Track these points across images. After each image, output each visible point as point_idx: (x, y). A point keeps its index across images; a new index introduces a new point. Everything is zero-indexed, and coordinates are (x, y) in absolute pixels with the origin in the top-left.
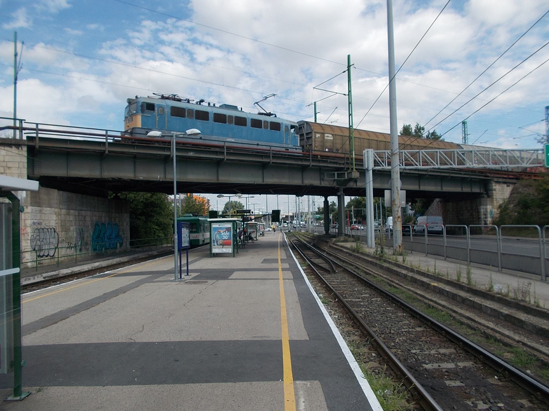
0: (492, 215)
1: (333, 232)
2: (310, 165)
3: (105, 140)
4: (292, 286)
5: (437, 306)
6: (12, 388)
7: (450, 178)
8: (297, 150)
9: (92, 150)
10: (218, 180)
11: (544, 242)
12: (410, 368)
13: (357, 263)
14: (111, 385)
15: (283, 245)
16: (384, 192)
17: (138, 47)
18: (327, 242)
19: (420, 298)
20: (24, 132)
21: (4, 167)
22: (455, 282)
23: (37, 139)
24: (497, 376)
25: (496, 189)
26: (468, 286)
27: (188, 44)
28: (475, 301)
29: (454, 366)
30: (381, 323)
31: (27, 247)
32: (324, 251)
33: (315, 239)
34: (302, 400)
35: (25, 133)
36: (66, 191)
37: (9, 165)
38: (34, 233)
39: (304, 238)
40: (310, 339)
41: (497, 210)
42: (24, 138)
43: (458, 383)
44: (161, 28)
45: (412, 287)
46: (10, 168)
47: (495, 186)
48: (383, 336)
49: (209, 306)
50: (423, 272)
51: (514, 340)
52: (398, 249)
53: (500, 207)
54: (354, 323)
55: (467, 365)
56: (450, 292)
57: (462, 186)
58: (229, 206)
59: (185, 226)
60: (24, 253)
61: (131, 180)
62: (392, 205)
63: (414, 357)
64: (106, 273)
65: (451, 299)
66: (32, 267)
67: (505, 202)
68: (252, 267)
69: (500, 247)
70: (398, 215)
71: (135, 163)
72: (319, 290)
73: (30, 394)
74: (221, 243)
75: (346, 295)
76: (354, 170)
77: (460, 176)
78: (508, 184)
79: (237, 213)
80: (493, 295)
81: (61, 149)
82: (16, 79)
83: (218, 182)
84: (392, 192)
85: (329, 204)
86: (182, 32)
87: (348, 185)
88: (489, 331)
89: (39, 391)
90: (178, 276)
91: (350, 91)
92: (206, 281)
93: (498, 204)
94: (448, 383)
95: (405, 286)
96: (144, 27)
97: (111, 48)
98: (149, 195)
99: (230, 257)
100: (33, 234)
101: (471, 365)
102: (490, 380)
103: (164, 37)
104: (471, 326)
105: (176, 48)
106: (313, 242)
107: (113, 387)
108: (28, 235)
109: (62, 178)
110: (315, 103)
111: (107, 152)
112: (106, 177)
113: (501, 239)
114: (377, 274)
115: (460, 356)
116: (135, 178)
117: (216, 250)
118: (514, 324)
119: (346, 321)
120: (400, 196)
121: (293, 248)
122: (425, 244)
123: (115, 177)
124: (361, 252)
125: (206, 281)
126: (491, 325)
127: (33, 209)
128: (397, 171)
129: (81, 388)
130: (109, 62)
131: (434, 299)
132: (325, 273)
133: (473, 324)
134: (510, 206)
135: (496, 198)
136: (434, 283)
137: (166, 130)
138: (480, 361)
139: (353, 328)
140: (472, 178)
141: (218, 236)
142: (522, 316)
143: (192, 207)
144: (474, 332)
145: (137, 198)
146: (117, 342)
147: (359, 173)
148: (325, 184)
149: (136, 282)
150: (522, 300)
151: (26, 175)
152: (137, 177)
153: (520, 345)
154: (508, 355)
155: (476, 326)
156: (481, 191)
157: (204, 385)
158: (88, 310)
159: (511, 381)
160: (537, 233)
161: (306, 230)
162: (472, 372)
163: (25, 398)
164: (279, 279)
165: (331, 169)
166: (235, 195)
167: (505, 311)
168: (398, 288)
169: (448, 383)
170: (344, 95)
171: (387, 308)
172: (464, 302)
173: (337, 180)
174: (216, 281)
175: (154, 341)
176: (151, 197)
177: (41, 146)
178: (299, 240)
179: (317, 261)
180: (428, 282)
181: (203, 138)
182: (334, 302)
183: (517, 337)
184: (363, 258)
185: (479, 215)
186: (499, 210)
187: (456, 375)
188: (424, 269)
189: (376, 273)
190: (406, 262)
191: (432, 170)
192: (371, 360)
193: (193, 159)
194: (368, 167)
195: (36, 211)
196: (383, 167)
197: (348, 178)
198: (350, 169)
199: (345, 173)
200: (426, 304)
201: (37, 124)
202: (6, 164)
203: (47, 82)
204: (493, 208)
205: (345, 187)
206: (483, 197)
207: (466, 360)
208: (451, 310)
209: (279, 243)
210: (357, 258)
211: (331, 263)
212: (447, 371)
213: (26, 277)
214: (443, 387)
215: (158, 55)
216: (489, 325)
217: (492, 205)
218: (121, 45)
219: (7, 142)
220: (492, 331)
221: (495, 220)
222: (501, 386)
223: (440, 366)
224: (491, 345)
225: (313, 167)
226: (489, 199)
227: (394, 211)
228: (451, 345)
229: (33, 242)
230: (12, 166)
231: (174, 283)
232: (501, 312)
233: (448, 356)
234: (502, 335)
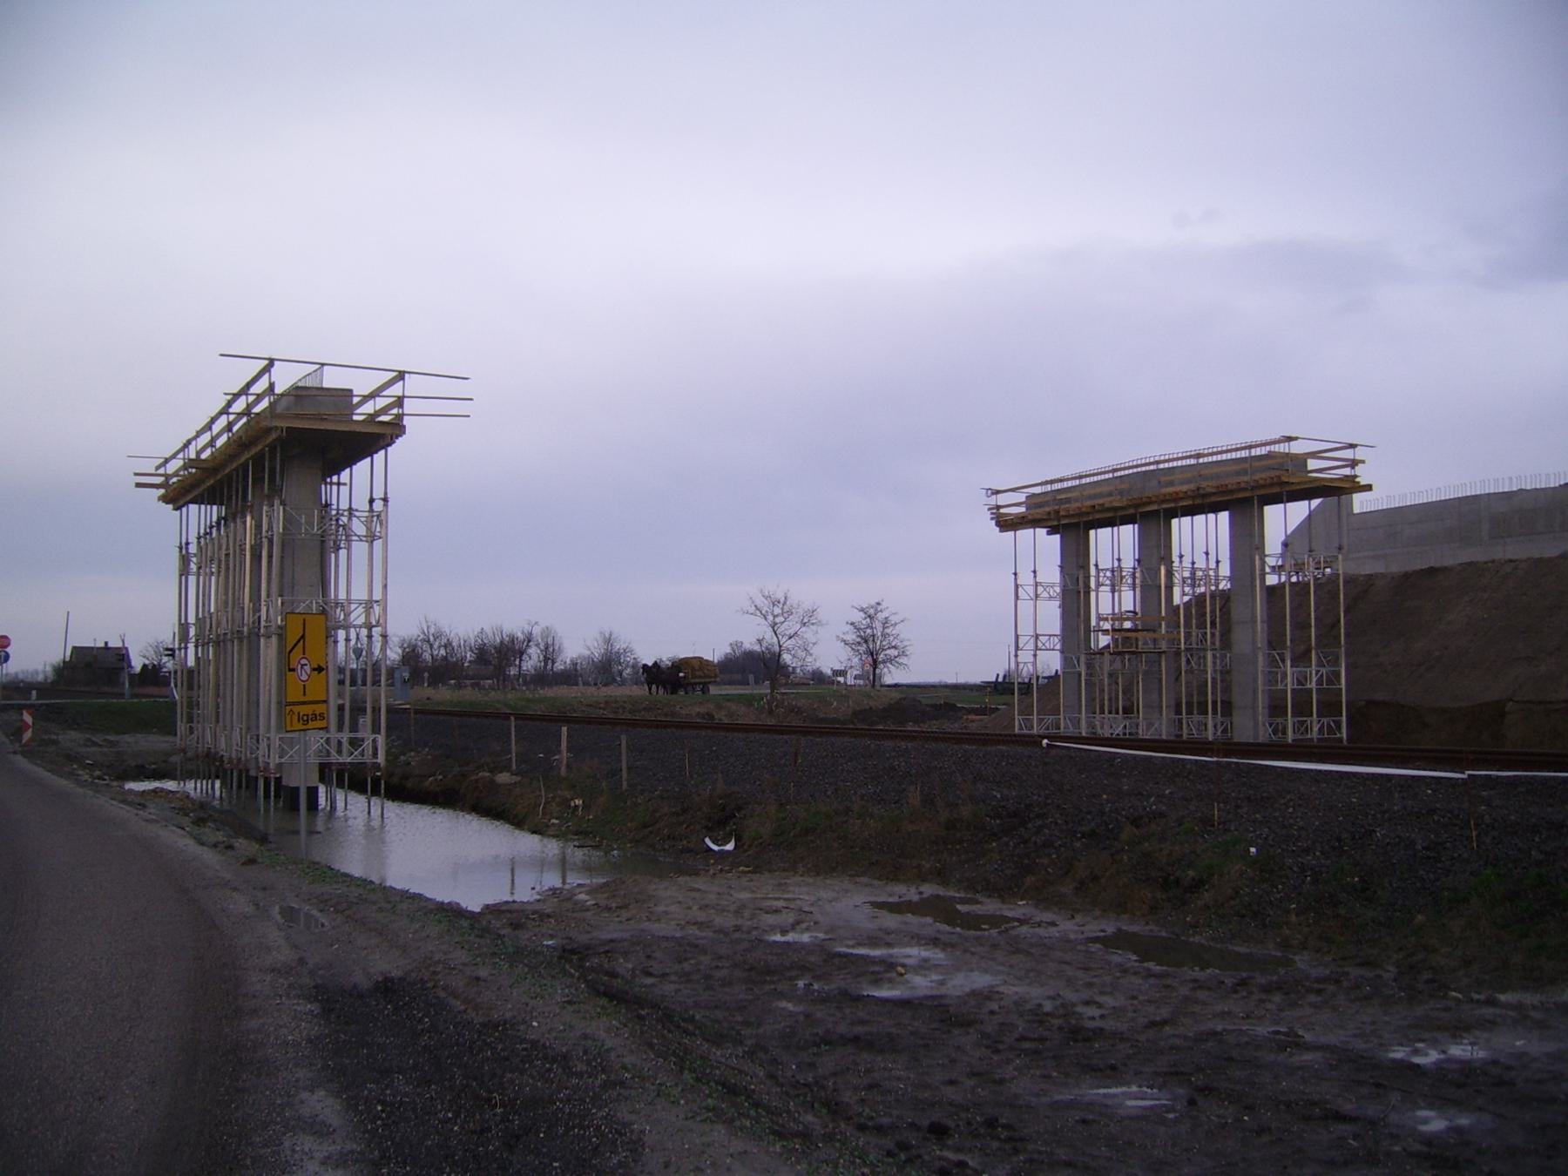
3: (345, 597)
8: (190, 541)
35: (292, 725)
118: (339, 721)
130: (1226, 673)
137: (1251, 465)
183: (211, 657)
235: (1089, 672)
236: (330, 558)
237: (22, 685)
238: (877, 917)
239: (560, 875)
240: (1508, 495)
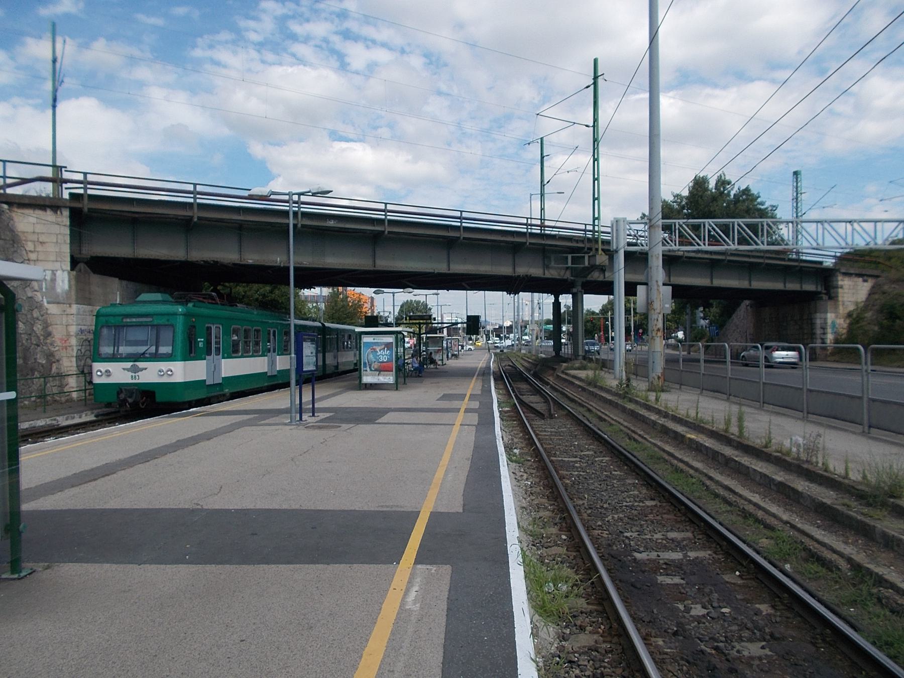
0: (835, 330)
1: (568, 354)
2: (526, 243)
4: (470, 436)
5: (687, 469)
7: (726, 262)
9: (172, 216)
10: (375, 266)
11: (869, 371)
12: (612, 557)
13: (591, 403)
14: (150, 564)
15: (484, 373)
16: (636, 288)
17: (255, 45)
18: (554, 369)
19: (667, 457)
20: (65, 186)
21: (34, 241)
22: (721, 433)
23: (86, 199)
24: (740, 572)
25: (844, 287)
26: (738, 440)
27: (336, 39)
28: (743, 462)
29: (681, 557)
30: (595, 494)
31: (72, 368)
32: (548, 384)
33: (537, 365)
34: (416, 588)
35: (66, 188)
36: (133, 281)
37: (42, 238)
38: (82, 346)
39: (522, 362)
40: (464, 512)
41: (844, 321)
42: (66, 195)
43: (677, 580)
44: (290, 13)
45: (660, 441)
46: (44, 243)
47: (842, 280)
48: (589, 511)
49: (330, 462)
50: (679, 418)
51: (780, 520)
52: (655, 383)
53: (849, 315)
54: (552, 493)
55: (700, 556)
56: (710, 448)
57: (785, 279)
58: (407, 308)
59: (309, 339)
60: (66, 377)
61: (235, 264)
62: (648, 309)
63: (623, 541)
64: (191, 410)
65: (710, 459)
66: (79, 399)
67: (858, 308)
68: (420, 406)
69: (807, 380)
70: (658, 327)
71: (240, 237)
72: (516, 443)
73: (34, 571)
74: (376, 367)
76: (600, 252)
77: (783, 263)
78: (865, 278)
79: (410, 319)
80: (769, 453)
81: (123, 214)
82: (55, 100)
83: (449, 272)
84: (649, 288)
85: (562, 311)
86: (326, 19)
87: (590, 276)
88: (750, 508)
89: (47, 569)
90: (295, 416)
91: (595, 120)
92: (340, 425)
93: (847, 311)
94: (660, 579)
95: (650, 440)
96: (264, 11)
97: (211, 47)
98: (268, 288)
99: (392, 390)
100: (80, 348)
101: (707, 556)
102: (727, 578)
103: (296, 28)
104: (727, 500)
105: (316, 46)
106: (534, 370)
107: (152, 566)
108: (73, 350)
109: (127, 261)
110: (542, 139)
111: (196, 220)
112: (194, 260)
113: (808, 366)
114: (615, 421)
115: (695, 543)
116: (241, 261)
117: (368, 378)
119: (540, 489)
120: (661, 296)
121: (498, 378)
122: (699, 373)
123: (209, 260)
124: (599, 386)
125: (340, 425)
126: (756, 498)
127: (79, 309)
128: (658, 254)
129: (107, 566)
131: (686, 459)
132: (537, 418)
133: (731, 496)
134: (866, 315)
135: (843, 301)
136: (691, 434)
138: (722, 550)
139: (548, 500)
140: (801, 267)
141: (371, 356)
142: (801, 485)
143: (340, 309)
144: (729, 508)
145: (248, 293)
146: (176, 507)
147: (607, 257)
148: (552, 273)
149: (231, 424)
150: (807, 461)
151: (69, 255)
152: (244, 260)
153: (787, 527)
154: (764, 542)
155: (734, 499)
156: (817, 287)
157: (282, 567)
158: (147, 463)
159: (758, 579)
160: (859, 356)
161: (530, 349)
162: (704, 565)
163: (26, 576)
164: (461, 425)
165: (562, 249)
166: (402, 290)
167: (780, 476)
168: (640, 443)
169: (660, 579)
170: (587, 126)
171: (613, 473)
172: (728, 465)
173: (572, 267)
174: (353, 425)
175: (231, 508)
176: (271, 292)
177: (92, 209)
178: (514, 367)
179: (527, 399)
180: (682, 433)
182: (533, 462)
183: (785, 517)
184: (600, 396)
185: (812, 329)
186: (848, 321)
187: (677, 569)
188: (682, 412)
189: (615, 418)
190: (659, 403)
191: (734, 252)
192: (558, 545)
193: (334, 231)
194: (617, 248)
195: (84, 311)
196: (699, 247)
197: (589, 264)
198: (594, 250)
199: (584, 257)
200: (673, 466)
201: (85, 174)
202: (36, 236)
203: (109, 103)
204: (837, 317)
205: (584, 280)
206: (821, 299)
207: (704, 548)
208: (706, 475)
209: (478, 369)
210: (593, 395)
211: (550, 400)
212: (666, 564)
213: (69, 414)
214: (649, 585)
215: (288, 58)
216: (752, 499)
217: (834, 313)
218: (227, 42)
219: (38, 203)
220: (755, 508)
221: (839, 337)
222: (739, 586)
223: (659, 556)
224: (747, 528)
225: (531, 246)
226: (830, 304)
227: (651, 319)
228: (690, 527)
229: (81, 361)
230: (48, 240)
231: (288, 428)
232: (773, 479)
233: (677, 542)
234: (767, 513)
235: (392, 637)
237: (853, 533)
238: (312, 528)
239: (52, 40)
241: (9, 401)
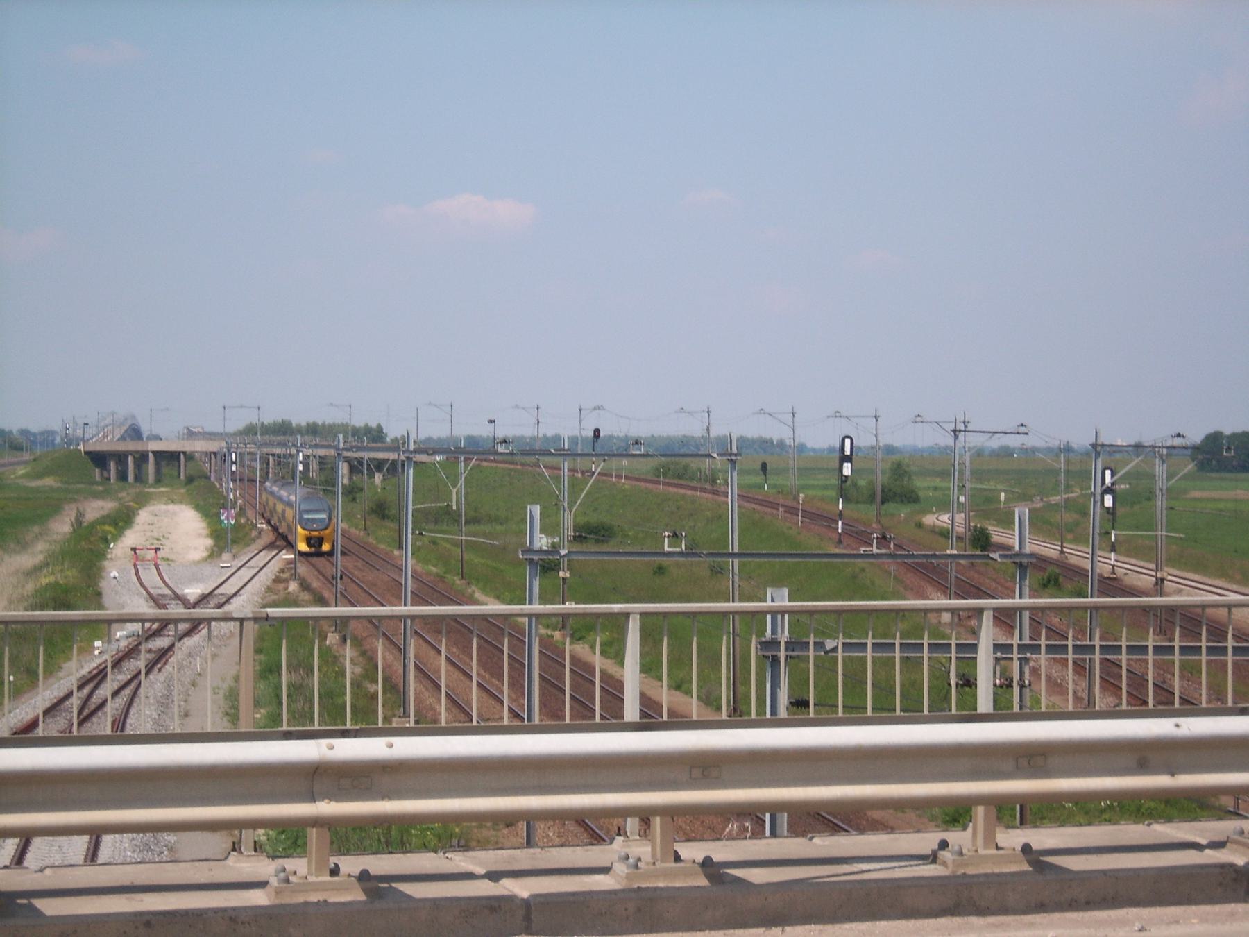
6: (231, 864)
75: (346, 828)
125: (849, 829)
181: (844, 414)
236: (110, 465)
239: (1051, 558)
240: (457, 758)
241: (838, 529)
